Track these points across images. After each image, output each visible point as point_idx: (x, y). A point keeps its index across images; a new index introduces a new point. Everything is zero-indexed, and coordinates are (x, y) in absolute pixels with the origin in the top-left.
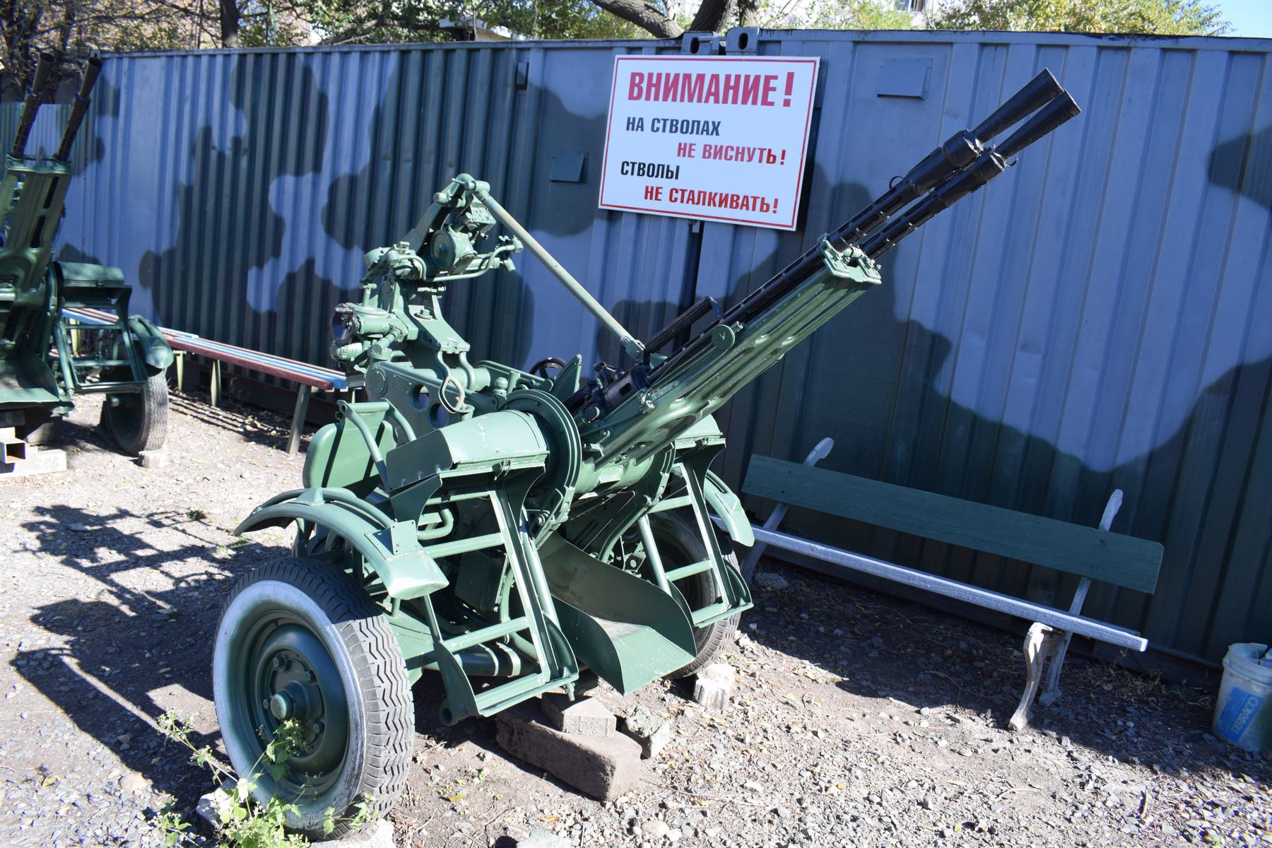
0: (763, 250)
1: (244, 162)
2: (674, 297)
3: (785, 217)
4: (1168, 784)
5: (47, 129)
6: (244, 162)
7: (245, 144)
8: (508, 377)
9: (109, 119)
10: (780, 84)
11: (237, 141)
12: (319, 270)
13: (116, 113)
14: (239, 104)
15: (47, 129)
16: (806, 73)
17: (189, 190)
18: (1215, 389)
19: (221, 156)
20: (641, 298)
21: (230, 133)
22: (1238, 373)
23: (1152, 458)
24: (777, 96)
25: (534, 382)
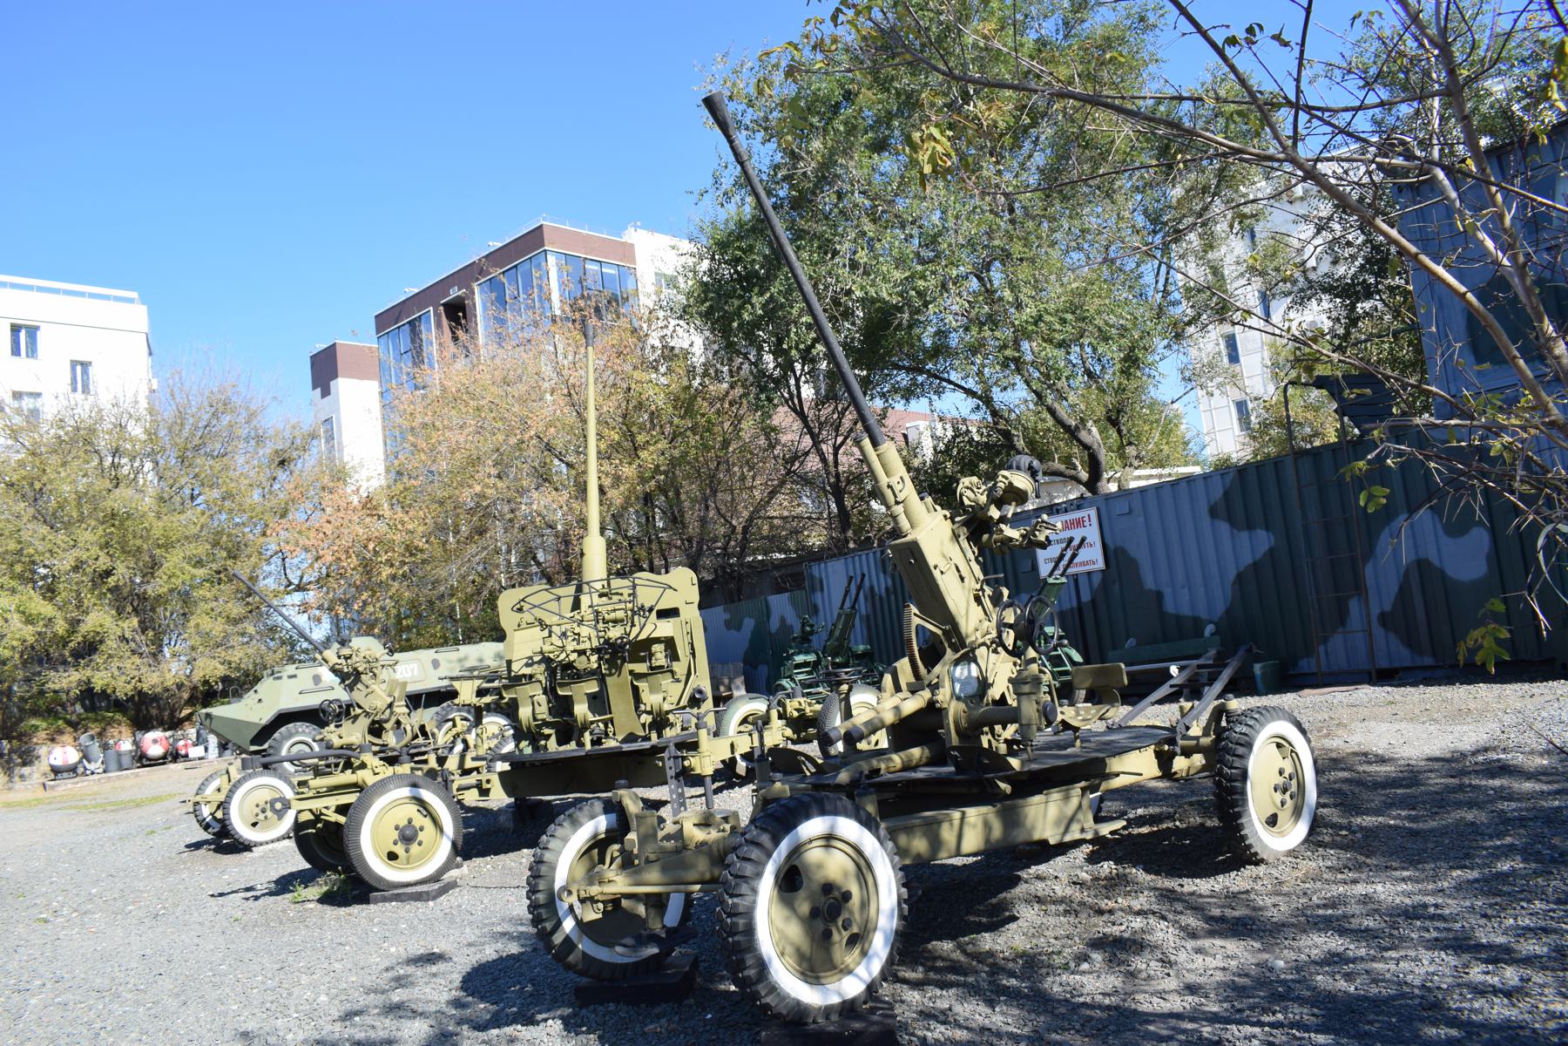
0: (1097, 580)
1: (893, 598)
2: (1075, 604)
3: (1101, 565)
4: (581, 622)
5: (886, 643)
6: (893, 598)
7: (892, 589)
8: (1407, 283)
9: (818, 595)
10: (1086, 519)
11: (887, 589)
12: (876, 589)
13: (822, 590)
14: (885, 572)
15: (886, 643)
16: (1093, 513)
17: (868, 617)
18: (1234, 583)
19: (881, 597)
20: (1065, 608)
21: (883, 586)
22: (1240, 577)
23: (1228, 611)
24: (1087, 523)
25: (1528, 281)
